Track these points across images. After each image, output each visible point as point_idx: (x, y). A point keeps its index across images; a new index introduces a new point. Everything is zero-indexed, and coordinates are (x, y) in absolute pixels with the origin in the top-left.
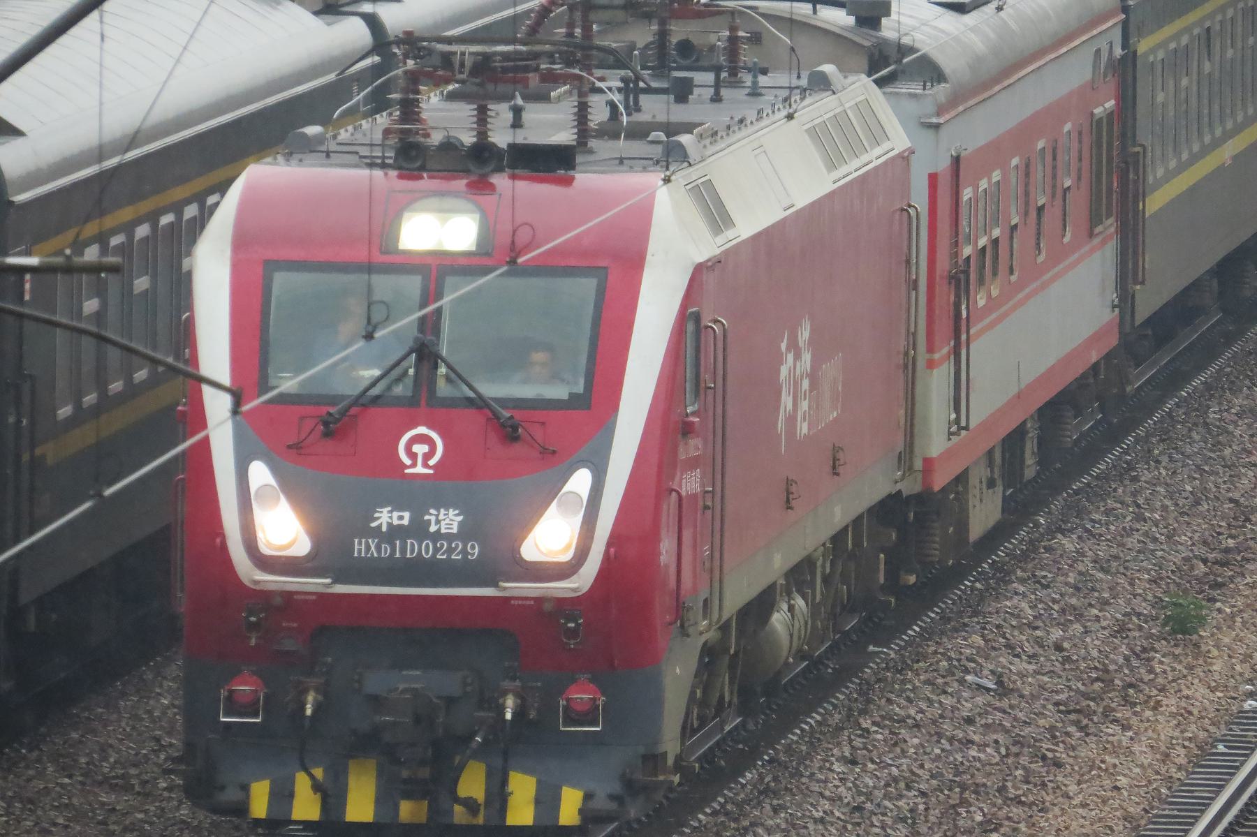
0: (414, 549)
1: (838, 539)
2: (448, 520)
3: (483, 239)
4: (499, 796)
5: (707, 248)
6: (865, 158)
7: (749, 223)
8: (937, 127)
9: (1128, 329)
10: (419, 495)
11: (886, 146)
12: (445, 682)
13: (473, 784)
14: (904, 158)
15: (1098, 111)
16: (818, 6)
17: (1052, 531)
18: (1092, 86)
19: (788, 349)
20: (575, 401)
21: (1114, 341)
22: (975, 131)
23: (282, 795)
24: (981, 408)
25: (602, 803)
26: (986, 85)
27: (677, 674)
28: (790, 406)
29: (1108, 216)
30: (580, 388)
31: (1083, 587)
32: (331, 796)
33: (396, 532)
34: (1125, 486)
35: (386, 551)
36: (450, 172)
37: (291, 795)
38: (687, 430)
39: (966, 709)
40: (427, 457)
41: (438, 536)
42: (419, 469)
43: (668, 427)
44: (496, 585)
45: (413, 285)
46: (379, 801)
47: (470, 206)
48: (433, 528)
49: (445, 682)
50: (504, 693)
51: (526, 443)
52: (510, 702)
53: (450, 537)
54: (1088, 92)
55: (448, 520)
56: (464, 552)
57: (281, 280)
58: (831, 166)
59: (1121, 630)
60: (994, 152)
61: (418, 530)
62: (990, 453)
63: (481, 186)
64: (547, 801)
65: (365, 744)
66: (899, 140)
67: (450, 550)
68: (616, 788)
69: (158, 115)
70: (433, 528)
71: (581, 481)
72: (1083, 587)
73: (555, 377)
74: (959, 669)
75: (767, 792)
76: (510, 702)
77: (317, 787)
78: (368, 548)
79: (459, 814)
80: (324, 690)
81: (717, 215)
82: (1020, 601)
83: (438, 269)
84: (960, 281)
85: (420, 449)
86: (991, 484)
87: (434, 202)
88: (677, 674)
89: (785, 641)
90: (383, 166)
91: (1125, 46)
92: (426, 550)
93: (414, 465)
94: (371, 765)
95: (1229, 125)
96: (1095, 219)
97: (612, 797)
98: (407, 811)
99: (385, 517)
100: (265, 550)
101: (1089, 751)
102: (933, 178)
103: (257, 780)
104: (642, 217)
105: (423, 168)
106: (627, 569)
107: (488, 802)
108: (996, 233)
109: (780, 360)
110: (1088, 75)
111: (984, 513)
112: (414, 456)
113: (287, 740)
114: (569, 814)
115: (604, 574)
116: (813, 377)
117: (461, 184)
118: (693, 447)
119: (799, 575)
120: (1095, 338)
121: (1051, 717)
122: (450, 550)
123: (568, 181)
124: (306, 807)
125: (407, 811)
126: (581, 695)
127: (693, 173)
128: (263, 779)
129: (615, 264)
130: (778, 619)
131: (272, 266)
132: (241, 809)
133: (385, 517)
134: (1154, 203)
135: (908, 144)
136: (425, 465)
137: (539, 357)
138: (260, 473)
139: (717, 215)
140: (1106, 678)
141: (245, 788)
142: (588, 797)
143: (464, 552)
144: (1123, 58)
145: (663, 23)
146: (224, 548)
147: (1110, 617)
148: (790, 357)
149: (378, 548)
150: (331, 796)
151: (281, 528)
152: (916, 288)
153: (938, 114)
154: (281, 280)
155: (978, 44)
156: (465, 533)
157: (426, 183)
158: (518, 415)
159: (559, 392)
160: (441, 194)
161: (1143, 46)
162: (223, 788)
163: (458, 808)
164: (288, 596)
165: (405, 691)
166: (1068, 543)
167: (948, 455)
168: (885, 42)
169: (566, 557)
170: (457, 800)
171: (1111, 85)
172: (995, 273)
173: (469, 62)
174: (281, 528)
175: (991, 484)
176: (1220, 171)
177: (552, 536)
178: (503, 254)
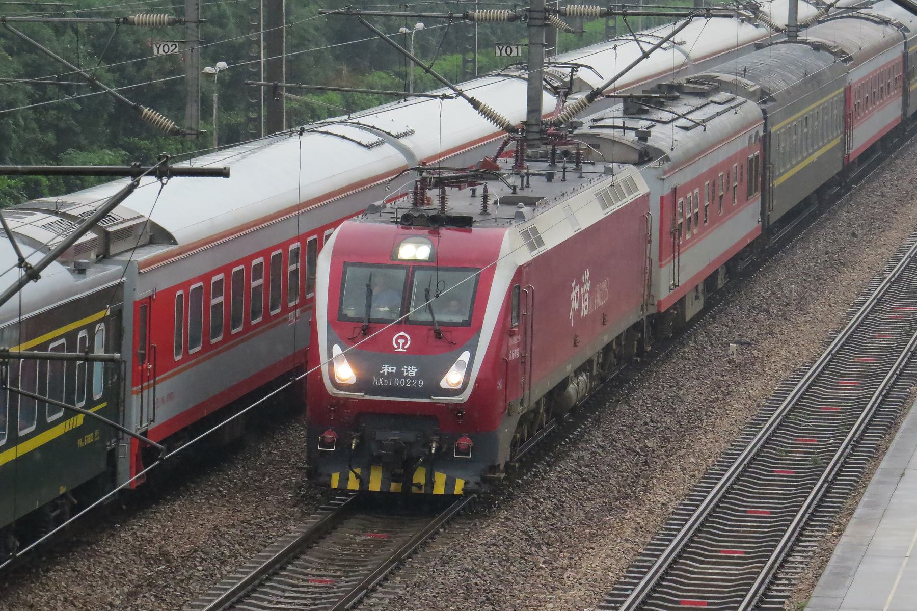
0: (397, 382)
1: (607, 349)
2: (412, 371)
3: (431, 256)
4: (430, 483)
5: (525, 256)
6: (613, 207)
7: (551, 242)
8: (663, 179)
9: (846, 162)
10: (399, 360)
11: (638, 193)
12: (410, 436)
13: (420, 477)
14: (646, 197)
15: (751, 156)
16: (487, 127)
17: (896, 158)
18: (749, 147)
19: (576, 285)
20: (466, 324)
21: (900, 121)
22: (680, 179)
23: (344, 479)
24: (684, 278)
25: (472, 486)
26: (702, 152)
27: (506, 431)
28: (577, 306)
29: (756, 190)
30: (467, 318)
31: (902, 171)
32: (364, 481)
33: (390, 374)
36: (426, 226)
37: (348, 479)
38: (512, 334)
39: (875, 200)
40: (404, 344)
41: (407, 377)
42: (401, 350)
43: (503, 332)
45: (402, 274)
46: (382, 484)
47: (427, 241)
49: (410, 436)
50: (432, 441)
51: (445, 339)
52: (434, 445)
53: (412, 378)
54: (750, 148)
55: (412, 371)
56: (417, 384)
57: (350, 270)
58: (604, 207)
59: (911, 182)
60: (697, 182)
61: (399, 374)
62: (697, 287)
63: (435, 232)
64: (450, 484)
65: (376, 460)
66: (643, 188)
67: (412, 383)
68: (478, 479)
71: (465, 356)
72: (902, 171)
73: (459, 312)
74: (873, 191)
75: (828, 219)
76: (434, 445)
77: (357, 476)
79: (414, 490)
80: (361, 438)
81: (533, 238)
82: (887, 175)
83: (414, 266)
84: (678, 231)
86: (697, 298)
87: (414, 239)
88: (506, 431)
89: (574, 397)
90: (397, 223)
91: (765, 130)
92: (402, 383)
94: (380, 469)
95: (816, 147)
96: (750, 193)
97: (477, 483)
98: (394, 487)
99: (386, 369)
100: (338, 381)
101: (904, 210)
102: (662, 198)
104: (498, 241)
105: (411, 224)
106: (483, 390)
107: (426, 484)
108: (697, 210)
109: (571, 290)
110: (747, 143)
111: (693, 309)
112: (398, 344)
113: (346, 459)
114: (458, 490)
115: (475, 390)
116: (591, 292)
117: (426, 232)
118: (515, 340)
119: (585, 367)
120: (896, 120)
121: (894, 202)
122: (412, 383)
123: (470, 231)
124: (353, 485)
125: (394, 487)
126: (464, 442)
127: (527, 226)
128: (336, 472)
129: (483, 265)
130: (571, 388)
131: (346, 264)
132: (328, 485)
133: (386, 369)
134: (777, 183)
135: (648, 190)
136: (403, 348)
137: (454, 303)
138: (337, 350)
139: (533, 238)
140: (907, 193)
141: (330, 476)
142: (466, 483)
143: (417, 384)
144: (764, 136)
145: (554, 146)
146: (321, 380)
147: (910, 178)
148: (577, 288)
150: (364, 481)
151: (345, 372)
152: (650, 242)
153: (664, 174)
154: (350, 270)
155: (691, 144)
156: (417, 377)
157: (413, 231)
158: (442, 328)
159: (458, 319)
160: (416, 236)
161: (773, 130)
162: (320, 475)
163: (413, 487)
164: (346, 400)
165: (392, 440)
166: (899, 161)
167: (669, 297)
168: (649, 147)
169: (459, 387)
170: (413, 484)
171: (759, 145)
172: (696, 224)
173: (433, 181)
174: (345, 372)
175: (697, 298)
176: (812, 163)
177: (453, 378)
178: (435, 263)
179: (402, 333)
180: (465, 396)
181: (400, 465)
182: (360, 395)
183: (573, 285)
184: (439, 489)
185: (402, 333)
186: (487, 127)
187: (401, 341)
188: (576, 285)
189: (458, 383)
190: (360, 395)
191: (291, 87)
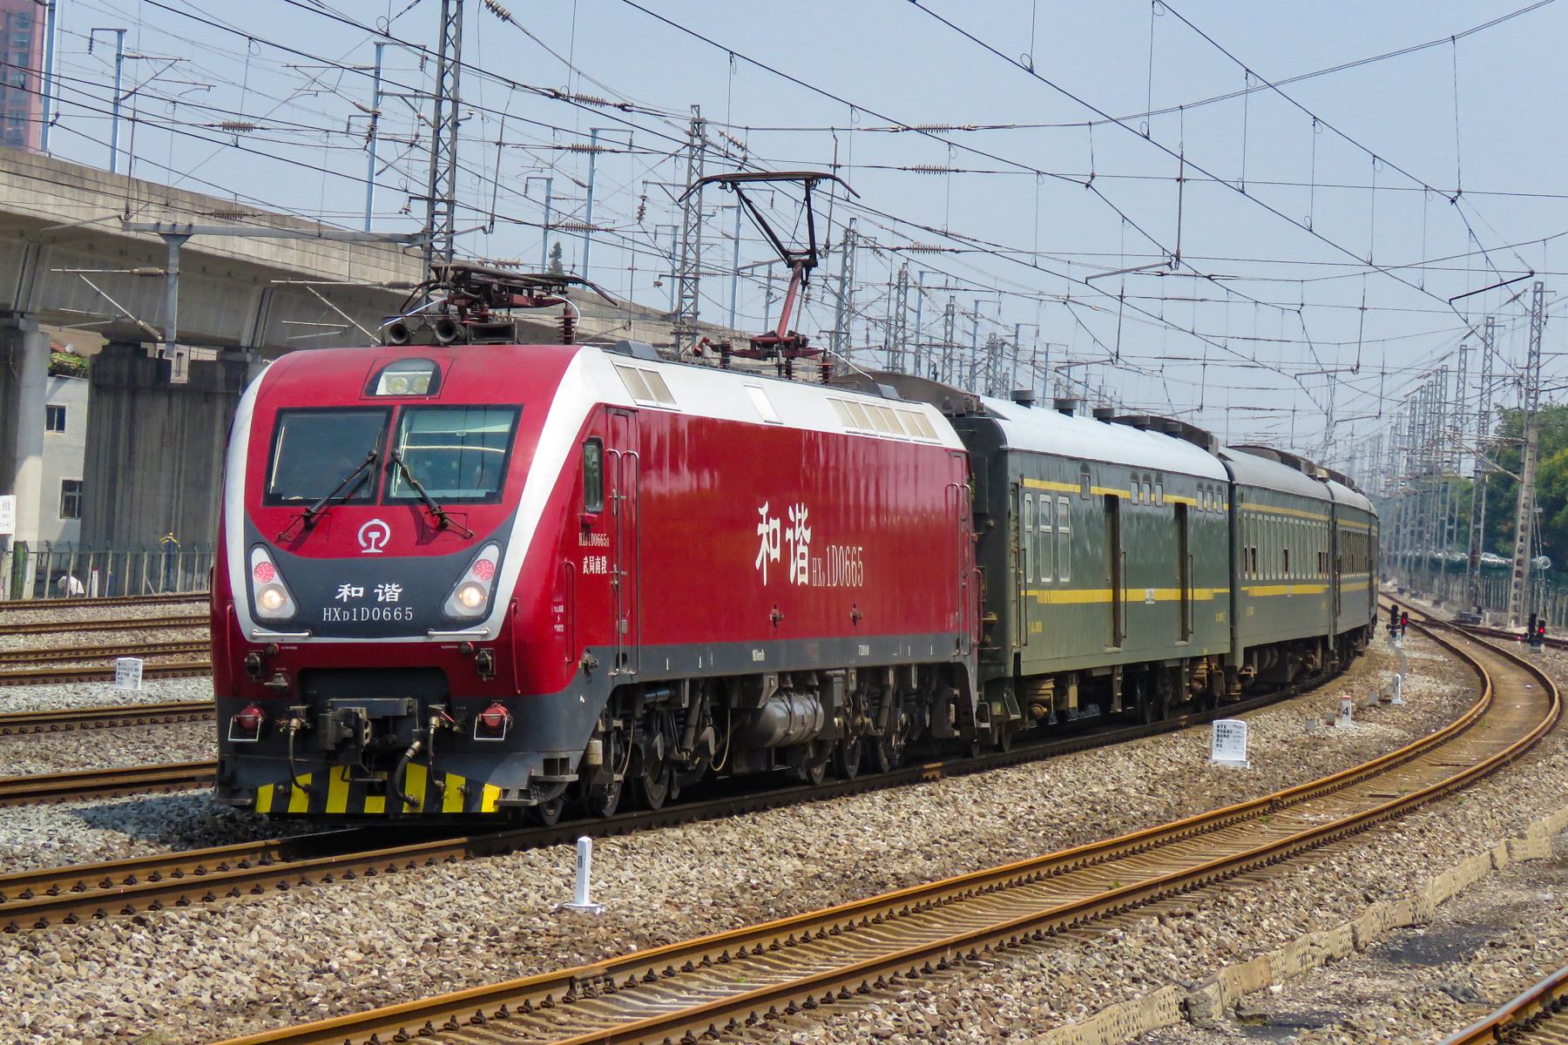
0: (366, 614)
2: (391, 592)
4: (435, 794)
16: (727, 325)
25: (514, 797)
32: (318, 795)
34: (787, 524)
35: (346, 616)
40: (379, 540)
41: (384, 604)
42: (373, 550)
44: (426, 634)
48: (380, 599)
53: (392, 605)
55: (391, 592)
61: (370, 600)
69: (319, 274)
70: (380, 599)
71: (490, 553)
77: (306, 789)
78: (333, 614)
85: (375, 534)
92: (377, 614)
93: (369, 547)
97: (521, 791)
98: (375, 805)
99: (346, 592)
103: (263, 784)
112: (368, 540)
124: (299, 804)
133: (346, 592)
136: (377, 547)
138: (260, 556)
142: (505, 792)
149: (341, 615)
150: (318, 795)
169: (484, 608)
177: (467, 599)
179: (376, 521)
180: (491, 629)
181: (379, 760)
182: (303, 636)
183: (763, 511)
184: (453, 804)
185: (376, 521)
186: (727, 325)
187: (374, 535)
188: (770, 515)
189: (480, 605)
190: (303, 636)
191: (150, 261)
